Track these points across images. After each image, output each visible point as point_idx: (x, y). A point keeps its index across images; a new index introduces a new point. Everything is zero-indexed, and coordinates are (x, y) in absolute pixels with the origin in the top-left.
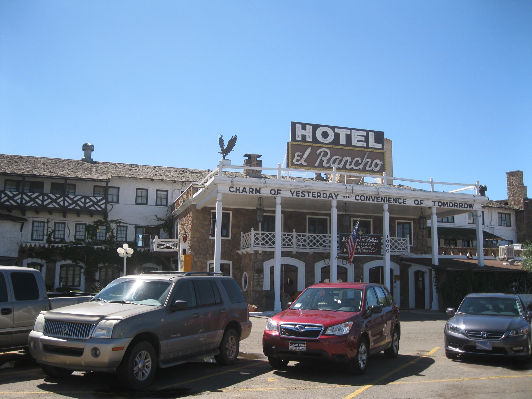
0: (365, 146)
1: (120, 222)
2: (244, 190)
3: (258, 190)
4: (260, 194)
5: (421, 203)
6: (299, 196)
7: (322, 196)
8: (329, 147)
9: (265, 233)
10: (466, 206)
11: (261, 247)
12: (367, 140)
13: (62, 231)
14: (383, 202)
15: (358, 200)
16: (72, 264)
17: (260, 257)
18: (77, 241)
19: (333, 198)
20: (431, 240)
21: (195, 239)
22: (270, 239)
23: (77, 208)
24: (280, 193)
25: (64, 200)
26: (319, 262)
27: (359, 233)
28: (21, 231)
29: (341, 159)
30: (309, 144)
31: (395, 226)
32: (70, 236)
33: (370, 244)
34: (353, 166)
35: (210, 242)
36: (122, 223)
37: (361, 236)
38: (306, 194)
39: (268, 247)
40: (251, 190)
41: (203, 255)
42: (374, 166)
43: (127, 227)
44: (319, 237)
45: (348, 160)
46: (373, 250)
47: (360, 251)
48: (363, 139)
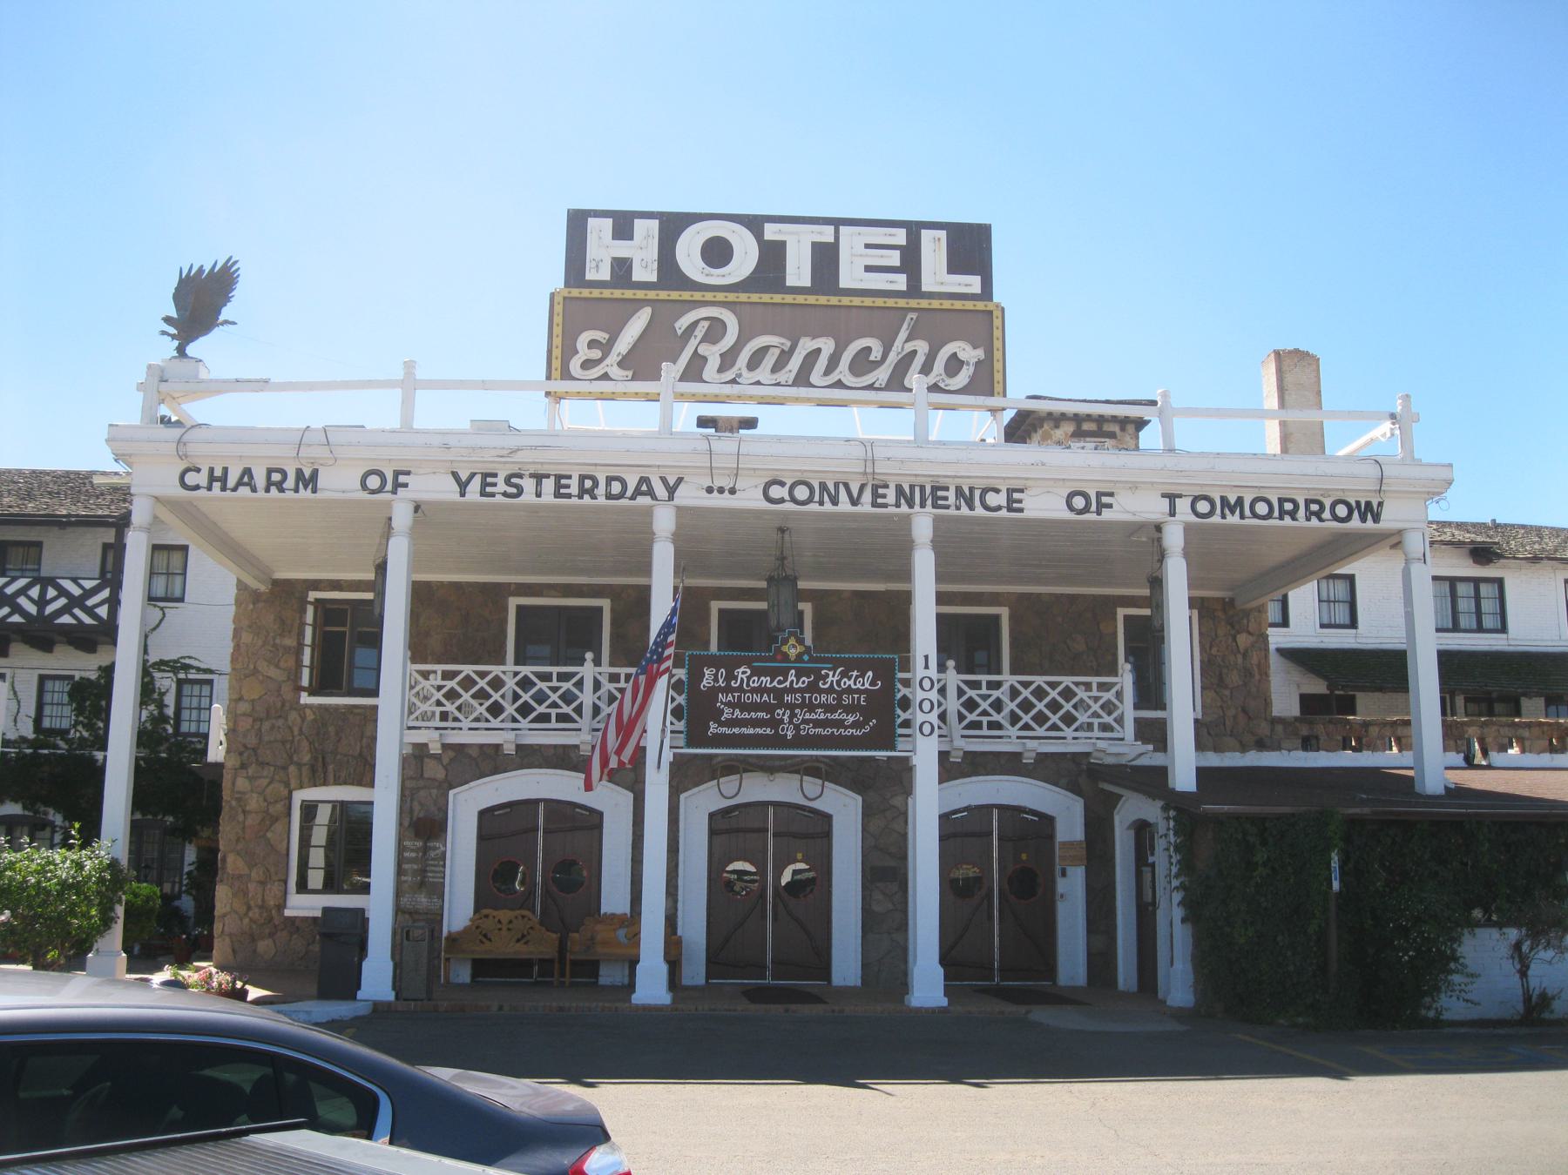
0: (904, 288)
1: (186, 667)
2: (246, 479)
3: (307, 473)
4: (314, 491)
5: (1101, 507)
6: (492, 495)
7: (601, 490)
8: (734, 303)
10: (1342, 511)
11: (530, 729)
12: (911, 261)
13: (187, 708)
14: (904, 508)
15: (782, 501)
16: (23, 816)
17: (434, 771)
18: (42, 737)
19: (654, 497)
20: (1407, 700)
21: (244, 707)
22: (1054, 706)
23: (16, 618)
24: (405, 485)
26: (696, 790)
27: (785, 648)
29: (786, 349)
30: (640, 294)
31: (1115, 634)
32: (18, 720)
33: (839, 699)
34: (843, 372)
35: (303, 719)
36: (194, 671)
37: (796, 661)
38: (528, 485)
39: (470, 729)
40: (276, 477)
41: (272, 769)
42: (942, 372)
43: (210, 682)
45: (819, 351)
47: (790, 734)
48: (894, 259)
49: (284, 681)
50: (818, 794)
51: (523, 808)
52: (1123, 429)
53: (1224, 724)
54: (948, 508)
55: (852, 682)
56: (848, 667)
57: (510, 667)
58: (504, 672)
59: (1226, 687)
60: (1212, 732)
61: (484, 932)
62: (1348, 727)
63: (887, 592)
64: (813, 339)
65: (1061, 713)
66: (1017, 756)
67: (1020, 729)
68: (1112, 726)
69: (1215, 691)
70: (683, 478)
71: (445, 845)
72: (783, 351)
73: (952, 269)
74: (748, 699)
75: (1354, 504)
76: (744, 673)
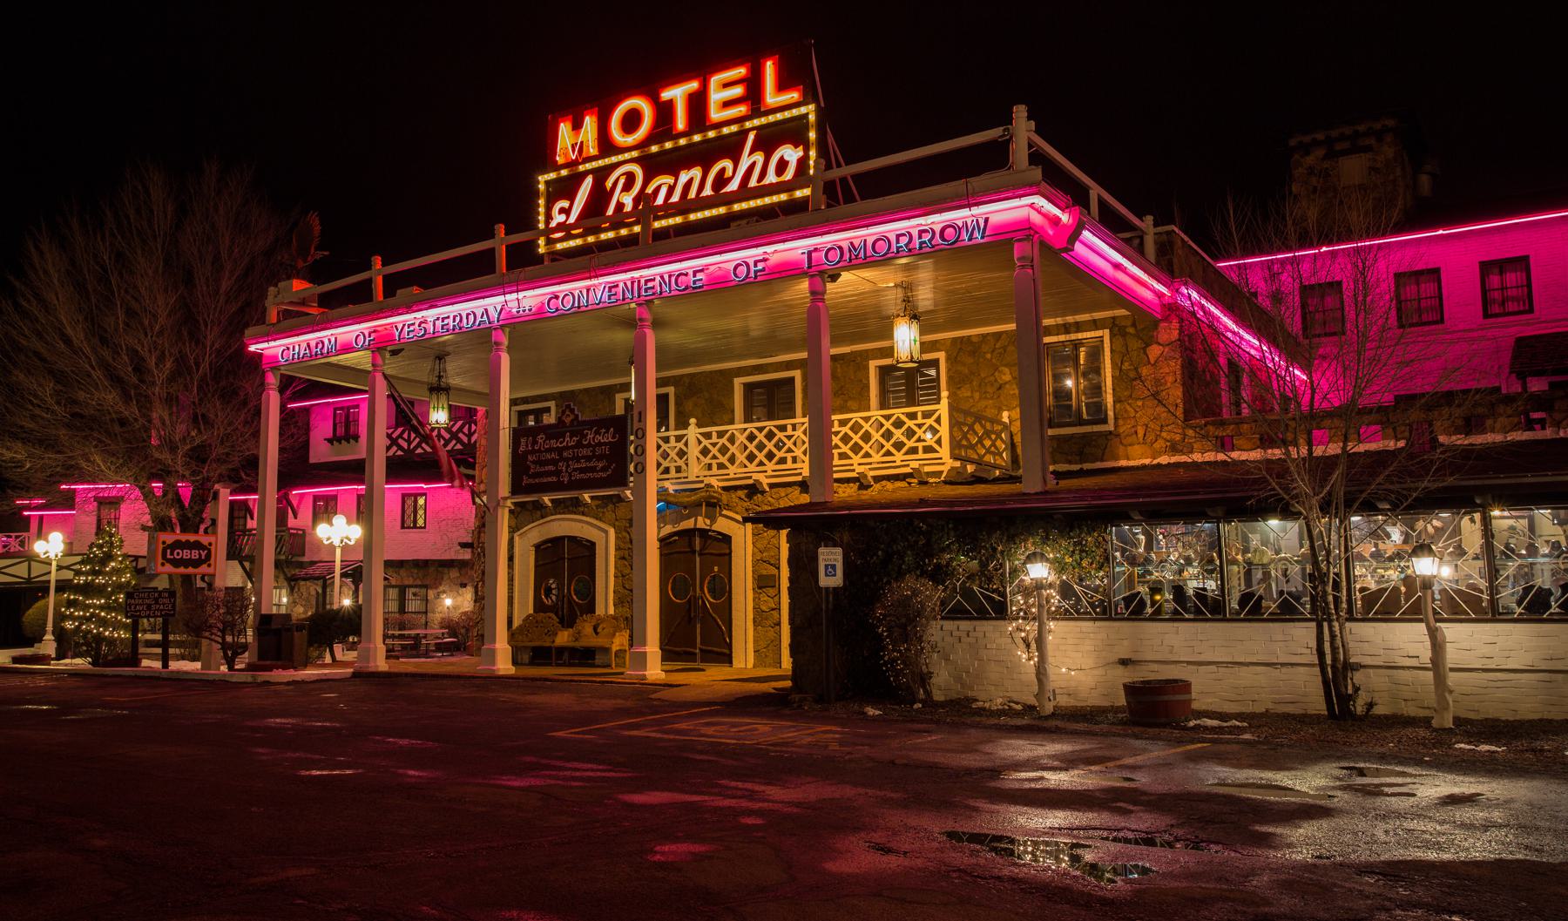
9: (728, 431)
33: (593, 451)
44: (891, 421)
46: (604, 469)
51: (557, 541)
67: (884, 456)
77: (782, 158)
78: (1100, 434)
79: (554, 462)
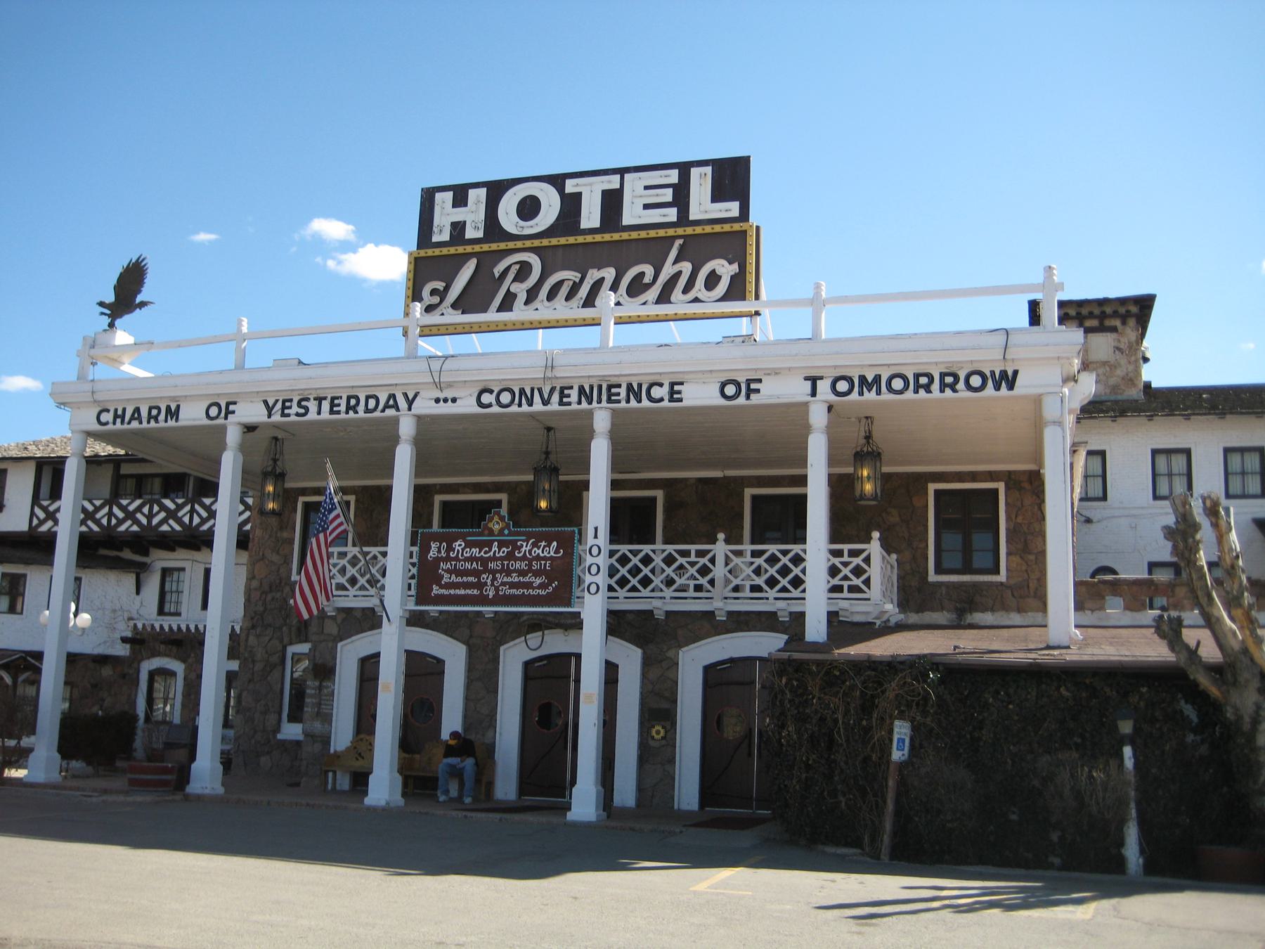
2: (136, 415)
5: (750, 392)
6: (288, 415)
7: (361, 408)
9: (618, 551)
10: (976, 381)
11: (752, 598)
14: (585, 405)
15: (490, 405)
17: (331, 628)
19: (398, 410)
22: (635, 571)
25: (192, 511)
26: (511, 643)
27: (491, 525)
28: (138, 592)
30: (469, 249)
33: (530, 565)
38: (312, 406)
48: (668, 195)
49: (282, 564)
50: (531, 647)
52: (1124, 323)
53: (1028, 587)
54: (570, 405)
55: (540, 551)
56: (539, 538)
57: (659, 546)
58: (654, 551)
59: (1030, 553)
60: (1016, 594)
61: (359, 752)
62: (1153, 588)
63: (725, 478)
64: (598, 270)
65: (791, 576)
66: (773, 615)
68: (761, 587)
69: (1021, 557)
70: (418, 393)
71: (334, 685)
72: (574, 282)
73: (716, 198)
74: (462, 566)
75: (988, 374)
76: (460, 545)
77: (713, 272)
78: (991, 584)
79: (476, 573)
